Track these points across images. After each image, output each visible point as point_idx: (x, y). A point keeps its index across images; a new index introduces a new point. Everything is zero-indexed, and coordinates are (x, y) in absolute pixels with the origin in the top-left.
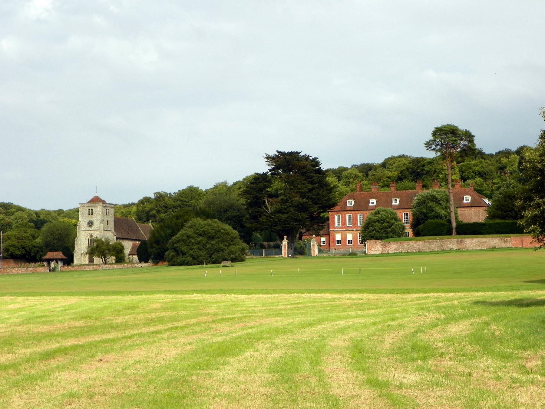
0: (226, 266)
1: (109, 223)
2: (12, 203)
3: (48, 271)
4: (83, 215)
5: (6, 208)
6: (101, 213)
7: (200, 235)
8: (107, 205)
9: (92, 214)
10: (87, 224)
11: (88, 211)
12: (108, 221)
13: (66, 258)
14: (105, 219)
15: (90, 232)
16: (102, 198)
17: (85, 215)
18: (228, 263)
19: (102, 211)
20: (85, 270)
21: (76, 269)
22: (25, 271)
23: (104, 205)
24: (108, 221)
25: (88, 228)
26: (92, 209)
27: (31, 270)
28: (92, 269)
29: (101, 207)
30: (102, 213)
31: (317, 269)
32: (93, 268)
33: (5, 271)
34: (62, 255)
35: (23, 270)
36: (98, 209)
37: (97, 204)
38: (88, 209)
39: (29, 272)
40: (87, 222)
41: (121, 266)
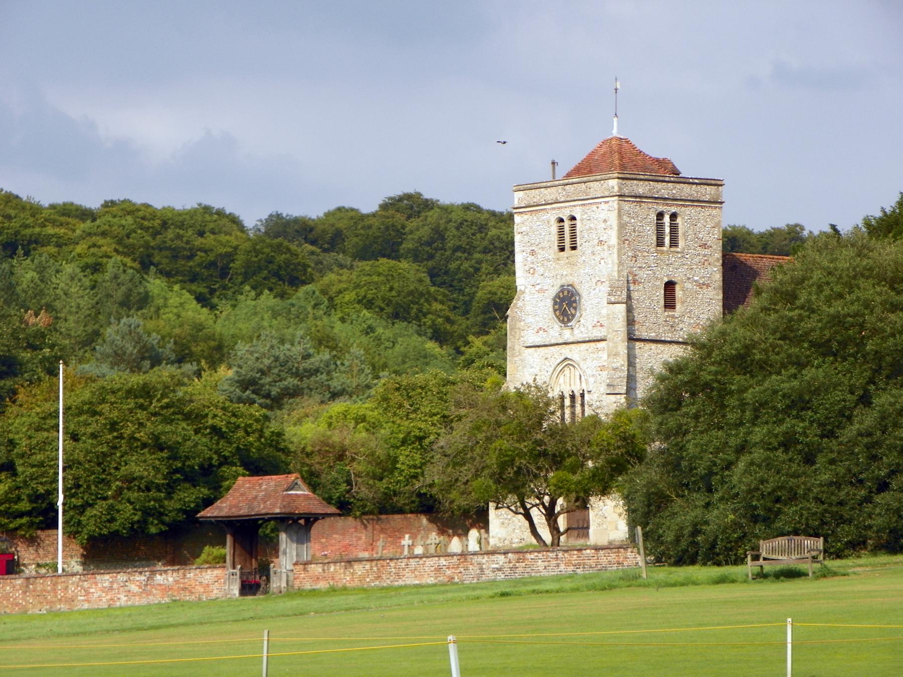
0: (791, 574)
1: (679, 293)
2: (438, 201)
3: (236, 591)
4: (533, 253)
5: (10, 199)
6: (614, 240)
7: (823, 348)
8: (687, 191)
9: (574, 248)
10: (550, 303)
11: (554, 229)
12: (670, 286)
13: (198, 515)
14: (643, 274)
15: (566, 351)
16: (653, 148)
17: (541, 254)
18: (800, 548)
19: (622, 226)
20: (401, 583)
21: (362, 578)
22: (140, 594)
23: (641, 188)
24: (670, 286)
25: (556, 332)
26: (573, 218)
27: (166, 589)
28: (431, 580)
29: (614, 202)
30: (623, 239)
31: (743, 623)
32: (439, 569)
33: (60, 594)
34: (303, 491)
35: (134, 588)
36: (603, 216)
37: (596, 188)
38: (552, 217)
39: (156, 598)
40: (553, 291)
41: (567, 565)
